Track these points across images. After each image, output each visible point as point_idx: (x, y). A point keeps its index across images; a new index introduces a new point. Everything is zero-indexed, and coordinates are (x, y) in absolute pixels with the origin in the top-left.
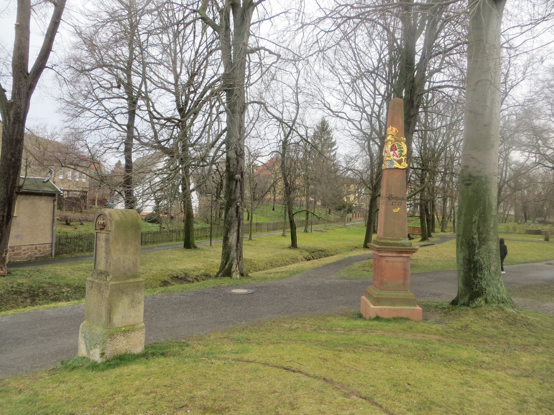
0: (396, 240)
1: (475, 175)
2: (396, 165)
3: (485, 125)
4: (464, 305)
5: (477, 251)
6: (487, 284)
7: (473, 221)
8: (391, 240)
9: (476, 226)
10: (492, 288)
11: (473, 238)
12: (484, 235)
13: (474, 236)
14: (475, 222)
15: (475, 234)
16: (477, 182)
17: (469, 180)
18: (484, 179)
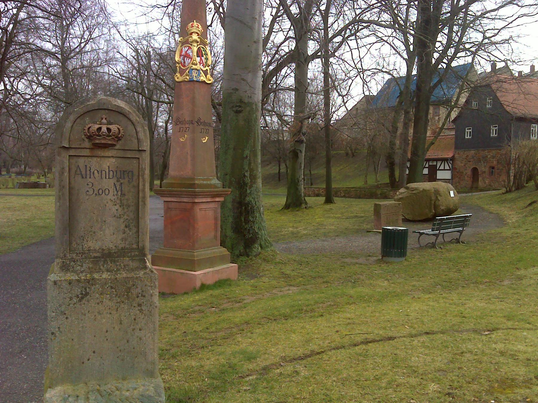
0: (208, 179)
2: (203, 78)
3: (255, 42)
5: (248, 191)
6: (259, 228)
8: (203, 180)
10: (263, 232)
11: (245, 176)
12: (255, 172)
14: (247, 157)
15: (247, 171)
16: (248, 109)
18: (254, 107)
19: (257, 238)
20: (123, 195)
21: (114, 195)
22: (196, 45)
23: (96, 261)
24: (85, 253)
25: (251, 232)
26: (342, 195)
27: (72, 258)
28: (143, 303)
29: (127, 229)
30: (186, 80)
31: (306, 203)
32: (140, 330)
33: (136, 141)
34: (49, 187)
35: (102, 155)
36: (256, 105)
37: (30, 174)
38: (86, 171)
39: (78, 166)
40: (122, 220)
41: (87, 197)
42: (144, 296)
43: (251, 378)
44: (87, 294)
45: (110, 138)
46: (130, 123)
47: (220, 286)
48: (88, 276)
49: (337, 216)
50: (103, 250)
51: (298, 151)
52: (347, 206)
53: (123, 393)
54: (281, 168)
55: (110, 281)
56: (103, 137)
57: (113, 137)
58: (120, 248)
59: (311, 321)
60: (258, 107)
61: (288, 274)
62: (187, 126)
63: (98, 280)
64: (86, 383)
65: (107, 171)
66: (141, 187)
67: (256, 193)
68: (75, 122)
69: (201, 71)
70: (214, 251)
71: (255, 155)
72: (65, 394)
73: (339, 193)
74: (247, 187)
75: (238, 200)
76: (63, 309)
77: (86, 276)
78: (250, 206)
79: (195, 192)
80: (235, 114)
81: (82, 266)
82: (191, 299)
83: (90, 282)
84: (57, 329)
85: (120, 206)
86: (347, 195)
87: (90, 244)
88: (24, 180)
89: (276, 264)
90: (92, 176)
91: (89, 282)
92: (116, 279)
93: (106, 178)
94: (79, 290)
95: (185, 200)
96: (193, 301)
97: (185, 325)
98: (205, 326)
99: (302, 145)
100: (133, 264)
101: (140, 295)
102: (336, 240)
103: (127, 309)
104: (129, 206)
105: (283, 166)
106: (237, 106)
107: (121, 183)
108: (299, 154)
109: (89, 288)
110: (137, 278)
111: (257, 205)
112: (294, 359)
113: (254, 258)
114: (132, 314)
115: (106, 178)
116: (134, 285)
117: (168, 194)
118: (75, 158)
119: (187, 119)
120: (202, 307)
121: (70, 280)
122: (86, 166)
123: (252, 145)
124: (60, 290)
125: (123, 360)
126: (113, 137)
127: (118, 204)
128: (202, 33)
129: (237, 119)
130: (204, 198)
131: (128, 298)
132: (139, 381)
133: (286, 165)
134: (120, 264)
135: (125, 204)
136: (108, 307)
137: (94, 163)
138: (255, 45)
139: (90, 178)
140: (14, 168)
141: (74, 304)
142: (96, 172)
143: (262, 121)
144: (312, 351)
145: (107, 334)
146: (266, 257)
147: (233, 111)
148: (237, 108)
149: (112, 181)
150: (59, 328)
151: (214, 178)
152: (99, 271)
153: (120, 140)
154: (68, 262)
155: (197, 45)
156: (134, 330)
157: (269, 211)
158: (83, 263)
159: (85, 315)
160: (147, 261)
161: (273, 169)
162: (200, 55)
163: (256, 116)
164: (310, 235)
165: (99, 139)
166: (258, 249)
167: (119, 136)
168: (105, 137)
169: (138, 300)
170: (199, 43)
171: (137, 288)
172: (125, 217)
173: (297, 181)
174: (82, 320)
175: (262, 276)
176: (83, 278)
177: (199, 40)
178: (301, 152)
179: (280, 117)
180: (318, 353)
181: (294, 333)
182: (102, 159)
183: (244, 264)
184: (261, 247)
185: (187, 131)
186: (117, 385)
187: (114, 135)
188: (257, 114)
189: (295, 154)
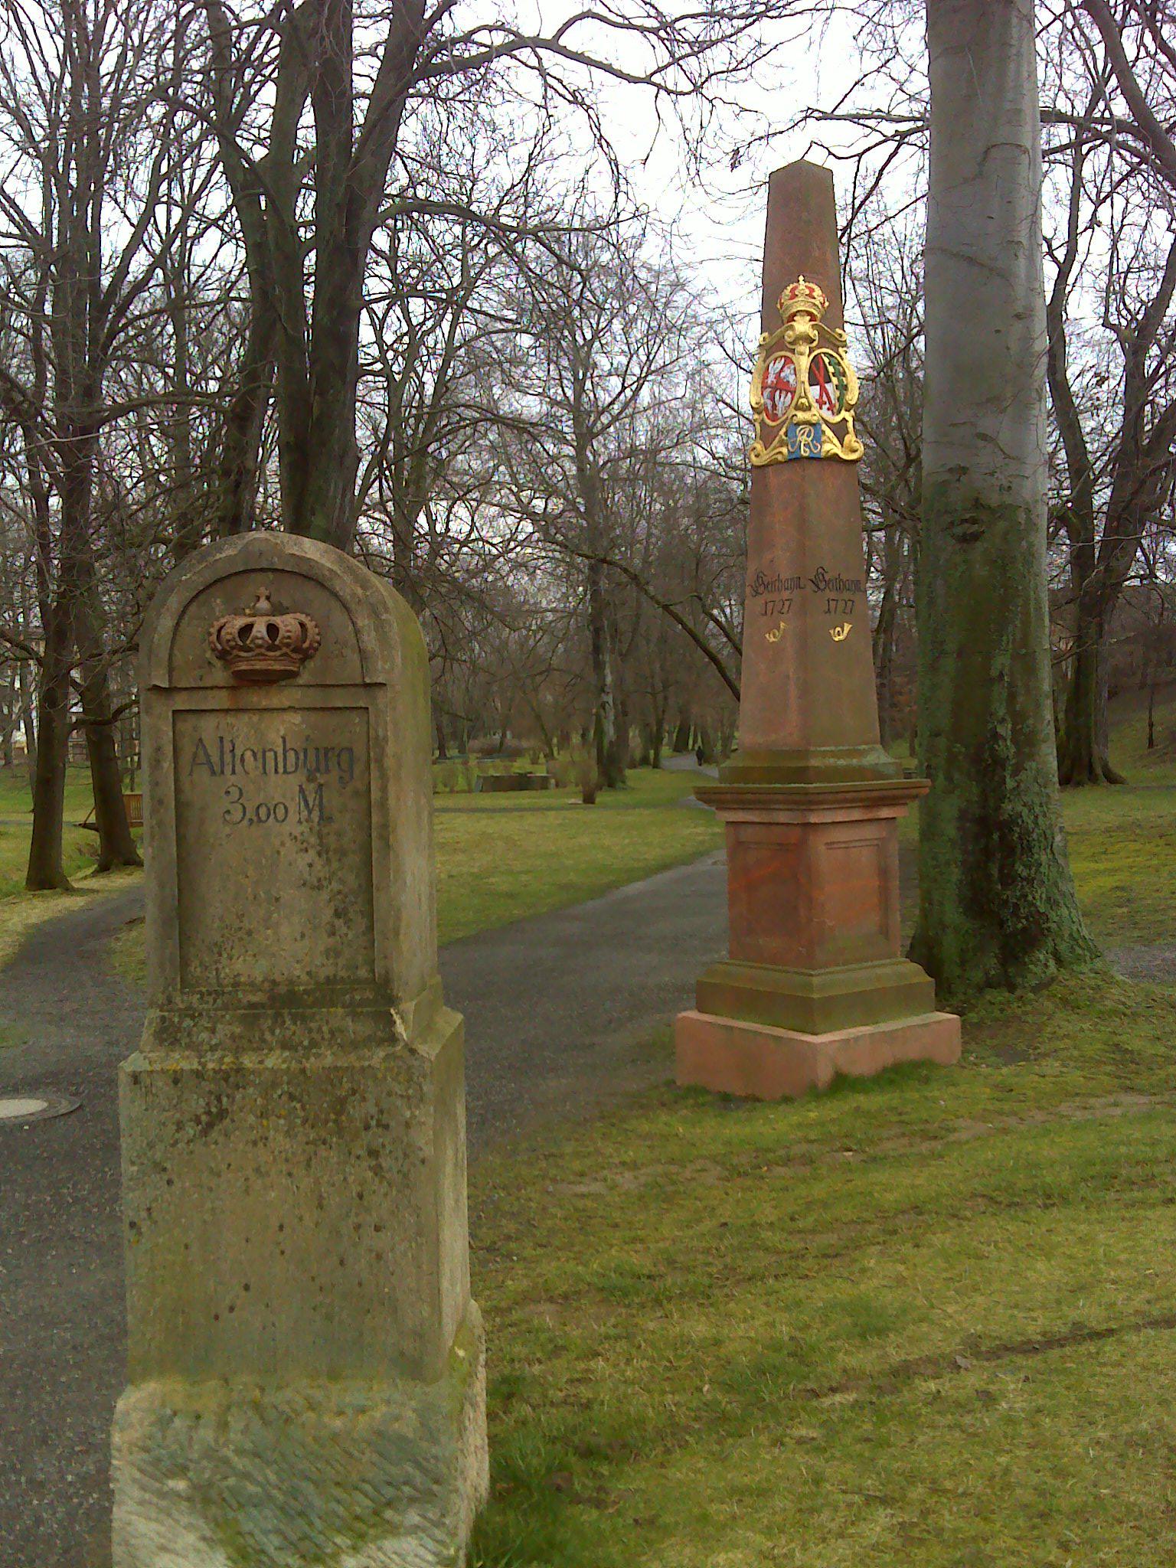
0: (849, 754)
1: (994, 499)
3: (1018, 316)
4: (989, 984)
5: (1010, 783)
6: (1049, 899)
7: (994, 673)
10: (1065, 912)
11: (996, 736)
12: (1031, 721)
13: (1000, 730)
14: (1001, 675)
15: (1003, 721)
16: (1002, 525)
17: (974, 521)
18: (1022, 517)
19: (1044, 933)
20: (325, 819)
21: (300, 822)
22: (804, 348)
23: (252, 1015)
24: (223, 993)
25: (1023, 911)
27: (189, 1008)
28: (383, 1146)
29: (339, 922)
30: (780, 457)
32: (377, 1229)
33: (356, 656)
34: (557, 785)
35: (264, 703)
36: (1028, 511)
37: (515, 754)
38: (222, 753)
39: (200, 740)
40: (325, 895)
41: (227, 830)
42: (386, 1127)
43: (837, 1398)
44: (222, 1114)
45: (278, 653)
46: (338, 604)
47: (892, 1082)
48: (226, 1060)
50: (274, 982)
53: (326, 1419)
55: (285, 1078)
56: (257, 651)
57: (285, 649)
58: (322, 978)
59: (1123, 1219)
61: (1132, 1052)
62: (786, 594)
63: (253, 1072)
64: (226, 1381)
65: (280, 751)
66: (375, 795)
67: (1036, 788)
68: (183, 612)
69: (824, 427)
70: (879, 971)
72: (163, 1405)
76: (158, 1156)
77: (221, 1059)
80: (958, 547)
81: (213, 1031)
82: (795, 1119)
83: (231, 1080)
84: (144, 1214)
85: (319, 854)
87: (239, 966)
88: (495, 768)
89: (1102, 1015)
90: (238, 768)
91: (226, 1080)
92: (303, 1071)
93: (276, 771)
94: (202, 1102)
95: (782, 817)
96: (800, 1125)
97: (738, 1201)
98: (790, 1210)
100: (356, 1028)
101: (373, 1123)
103: (338, 1163)
104: (342, 853)
107: (321, 786)
109: (228, 1096)
110: (363, 1069)
112: (1007, 1349)
113: (1031, 995)
114: (351, 1179)
115: (276, 771)
116: (354, 1092)
117: (785, 802)
118: (190, 716)
119: (785, 575)
120: (814, 1149)
121: (175, 1072)
122: (221, 739)
124: (150, 1098)
125: (329, 1317)
126: (285, 649)
127: (313, 847)
130: (828, 813)
131: (340, 1131)
132: (375, 1387)
134: (320, 1030)
135: (333, 846)
136: (283, 1155)
137: (242, 728)
138: (1018, 327)
139: (234, 772)
140: (475, 738)
141: (188, 1142)
142: (248, 754)
144: (1077, 1325)
145: (281, 1237)
149: (295, 780)
150: (149, 1209)
151: (872, 749)
152: (262, 1046)
153: (311, 657)
154: (176, 1020)
155: (811, 351)
156: (358, 1227)
157: (1162, 842)
158: (215, 1023)
159: (219, 1176)
160: (396, 1018)
162: (822, 380)
163: (1031, 545)
165: (248, 659)
166: (1046, 966)
167: (305, 645)
168: (263, 651)
169: (366, 1138)
171: (364, 1099)
172: (335, 886)
174: (211, 1189)
175: (1045, 1055)
176: (210, 1066)
177: (813, 334)
180: (1097, 1335)
181: (1048, 1256)
182: (266, 715)
183: (997, 1013)
184: (1059, 961)
185: (785, 610)
186: (310, 1392)
187: (288, 645)
188: (1032, 539)
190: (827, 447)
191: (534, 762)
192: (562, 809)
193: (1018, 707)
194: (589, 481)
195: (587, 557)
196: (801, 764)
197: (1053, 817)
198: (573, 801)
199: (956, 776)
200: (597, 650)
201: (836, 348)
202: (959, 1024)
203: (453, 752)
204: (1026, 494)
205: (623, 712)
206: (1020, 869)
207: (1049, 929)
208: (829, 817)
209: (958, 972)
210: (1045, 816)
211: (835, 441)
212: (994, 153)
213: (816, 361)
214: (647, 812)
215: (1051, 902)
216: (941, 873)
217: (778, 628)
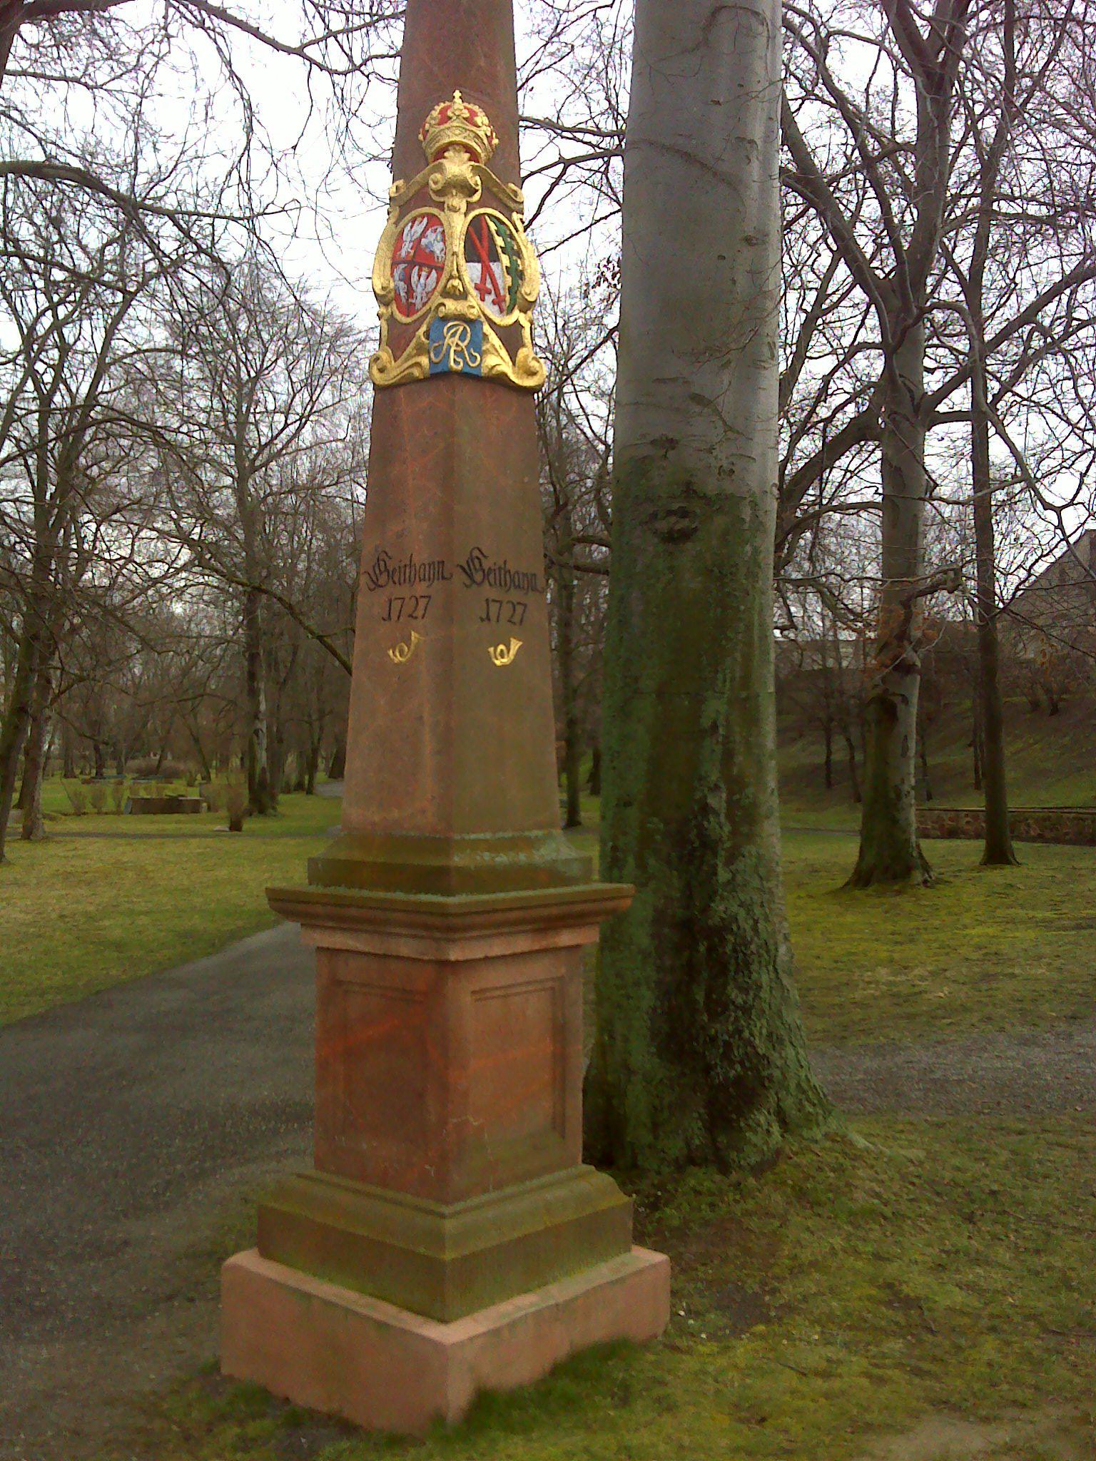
0: (513, 844)
1: (711, 486)
2: (497, 360)
3: (748, 241)
4: (692, 1160)
5: (723, 875)
6: (770, 1035)
7: (706, 723)
8: (493, 847)
9: (719, 749)
10: (790, 1052)
11: (705, 809)
12: (750, 791)
13: (712, 801)
14: (715, 726)
15: (716, 788)
16: (720, 522)
17: (684, 513)
18: (747, 513)
19: (762, 1082)
25: (737, 1053)
26: (1032, 833)
30: (416, 373)
31: (926, 868)
34: (209, 809)
36: (755, 505)
37: (171, 776)
49: (1039, 915)
51: (897, 700)
52: (1060, 876)
54: (834, 747)
60: (761, 513)
62: (421, 588)
67: (756, 883)
69: (487, 328)
71: (753, 721)
73: (1023, 827)
74: (715, 855)
75: (680, 912)
78: (731, 938)
79: (442, 911)
86: (1048, 835)
95: (406, 947)
99: (908, 679)
102: (1077, 1039)
105: (839, 743)
106: (670, 513)
108: (901, 707)
111: (764, 935)
117: (410, 925)
119: (422, 556)
123: (737, 675)
128: (495, 150)
129: (671, 569)
133: (848, 740)
140: (133, 758)
143: (777, 616)
146: (808, 1177)
147: (655, 532)
148: (673, 519)
155: (470, 206)
161: (810, 753)
162: (485, 257)
164: (965, 1009)
170: (476, 197)
173: (893, 795)
177: (475, 181)
178: (905, 700)
179: (831, 600)
183: (706, 1212)
184: (784, 1123)
185: (420, 613)
189: (887, 710)
190: (491, 360)
191: (190, 785)
192: (206, 836)
193: (735, 771)
194: (249, 512)
195: (242, 584)
196: (437, 862)
197: (776, 920)
198: (218, 827)
199: (652, 862)
200: (252, 676)
201: (508, 211)
202: (666, 1270)
203: (110, 771)
204: (754, 484)
205: (277, 740)
206: (734, 994)
207: (770, 1078)
208: (476, 951)
209: (647, 1138)
210: (767, 919)
211: (503, 352)
212: (723, 17)
213: (476, 231)
214: (292, 842)
215: (774, 1039)
216: (629, 997)
217: (407, 640)
